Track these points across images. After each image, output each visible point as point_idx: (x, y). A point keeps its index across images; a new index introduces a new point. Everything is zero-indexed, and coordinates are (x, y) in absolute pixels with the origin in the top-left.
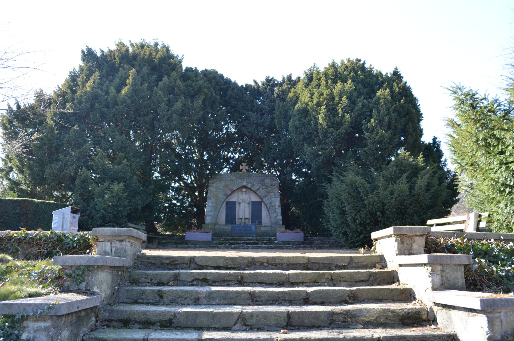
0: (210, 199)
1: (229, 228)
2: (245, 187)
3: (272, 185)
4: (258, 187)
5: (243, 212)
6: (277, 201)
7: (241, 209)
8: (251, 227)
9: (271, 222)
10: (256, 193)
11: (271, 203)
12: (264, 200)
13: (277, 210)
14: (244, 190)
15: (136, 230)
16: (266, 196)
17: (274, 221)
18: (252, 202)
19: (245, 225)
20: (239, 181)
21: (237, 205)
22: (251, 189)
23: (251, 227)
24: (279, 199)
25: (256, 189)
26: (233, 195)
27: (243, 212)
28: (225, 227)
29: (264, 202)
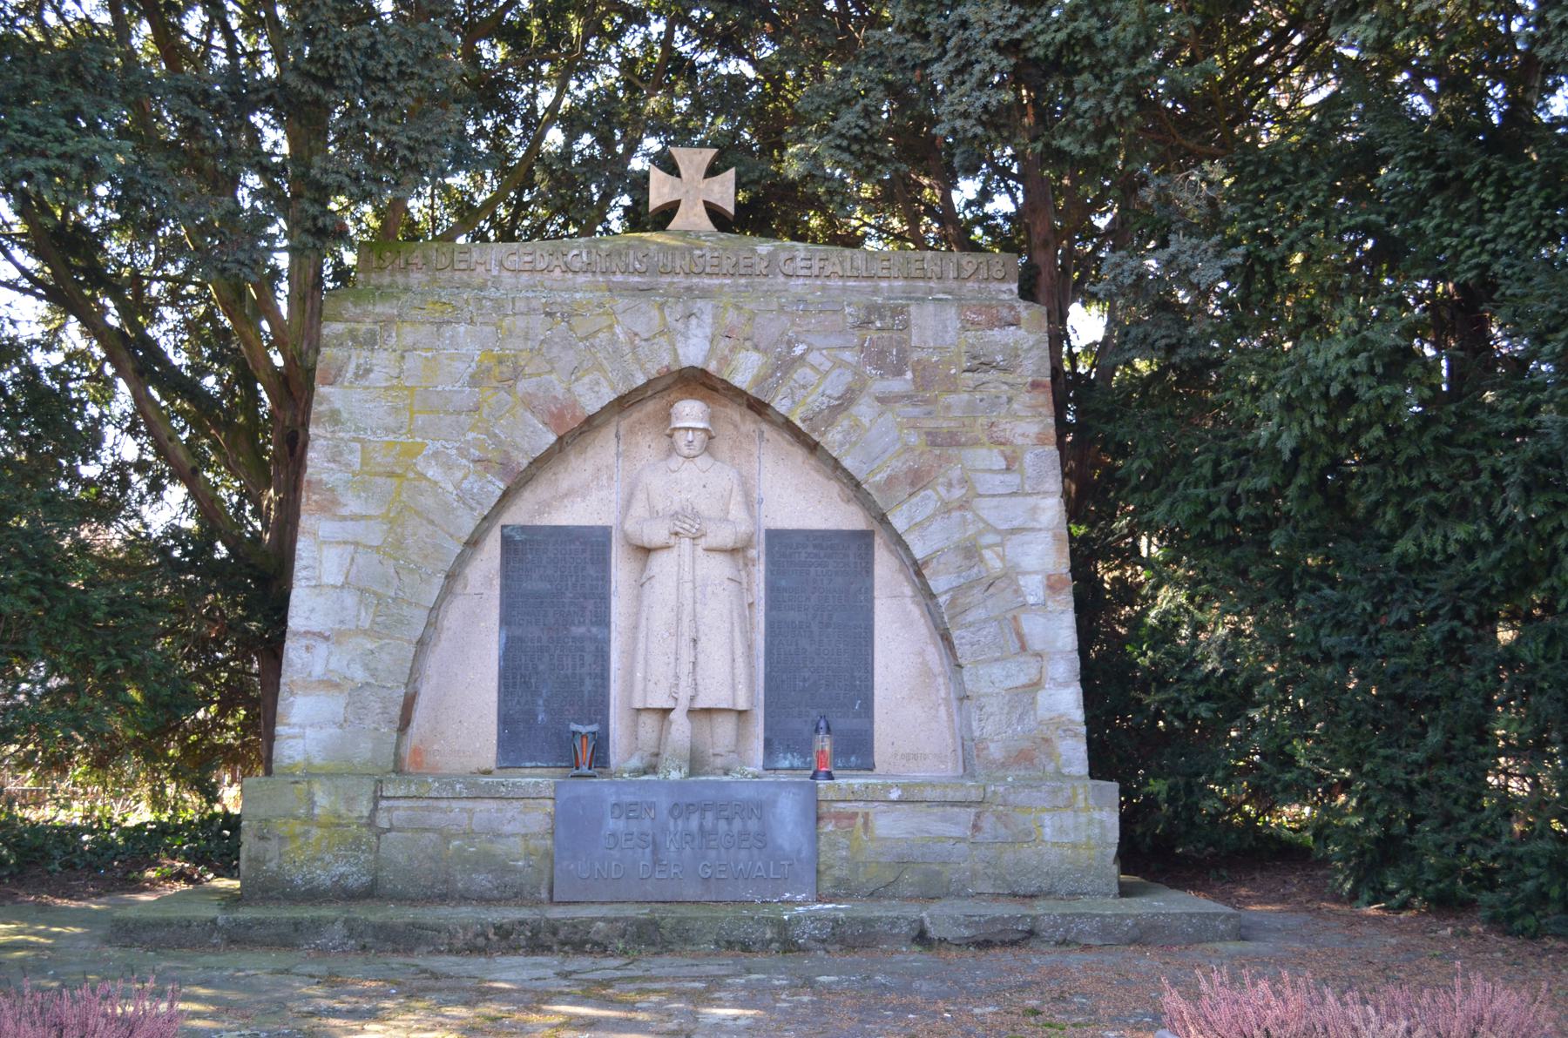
0: (329, 506)
1: (519, 818)
2: (697, 382)
3: (981, 364)
4: (835, 385)
5: (684, 644)
6: (1031, 530)
7: (659, 616)
8: (758, 808)
9: (969, 752)
10: (813, 447)
11: (970, 552)
12: (899, 521)
13: (1032, 626)
14: (690, 412)
15: (847, 463)
16: (917, 480)
17: (997, 732)
18: (775, 538)
19: (706, 805)
20: (641, 319)
21: (621, 571)
22: (758, 407)
23: (758, 808)
24: (1051, 509)
25: (816, 400)
26: (579, 469)
27: (684, 644)
28: (485, 809)
29: (898, 542)
